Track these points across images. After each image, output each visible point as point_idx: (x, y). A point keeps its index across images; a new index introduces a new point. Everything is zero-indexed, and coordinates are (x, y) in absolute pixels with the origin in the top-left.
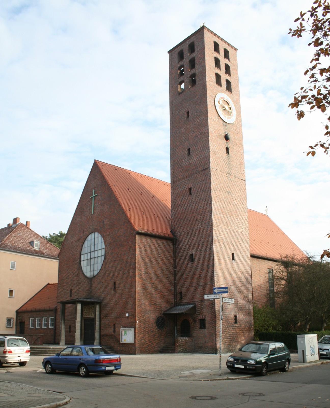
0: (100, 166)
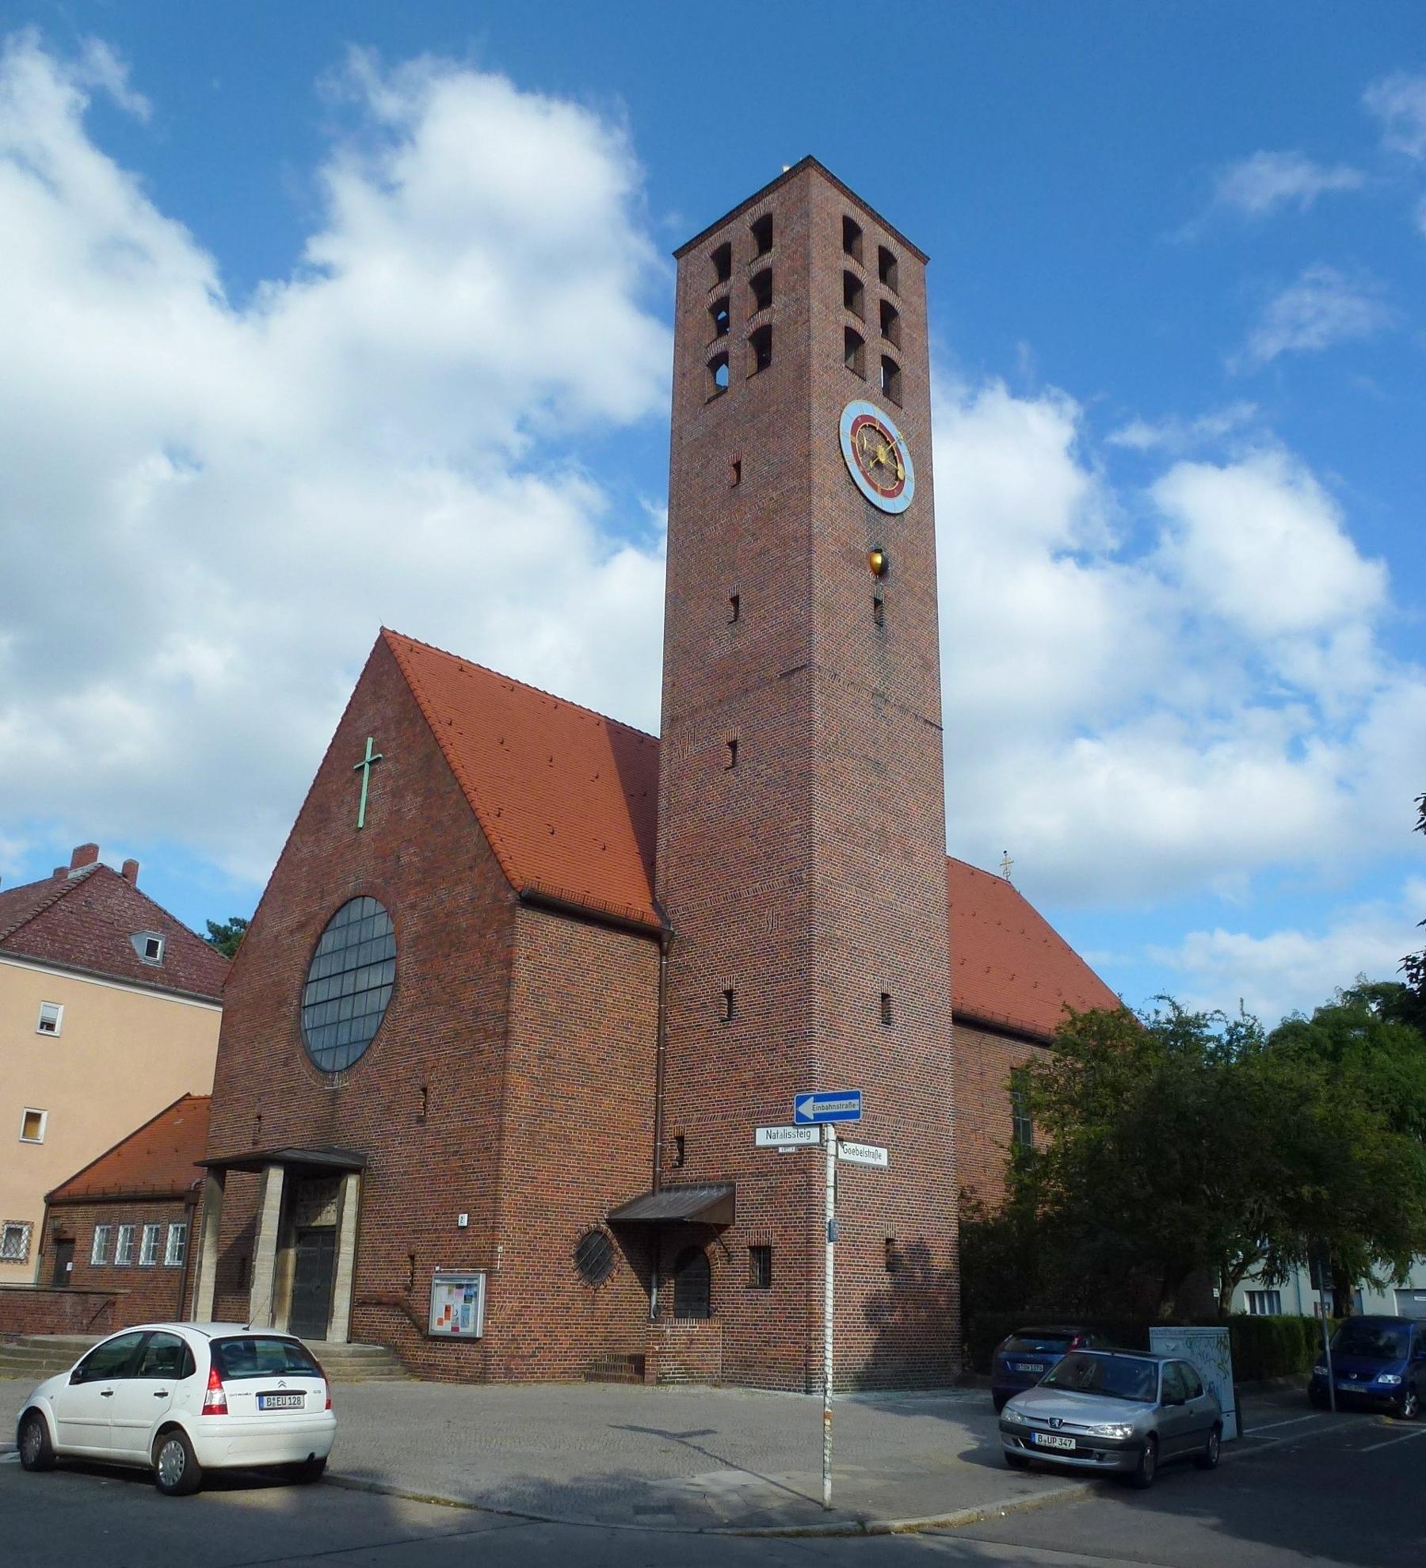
0: (401, 652)
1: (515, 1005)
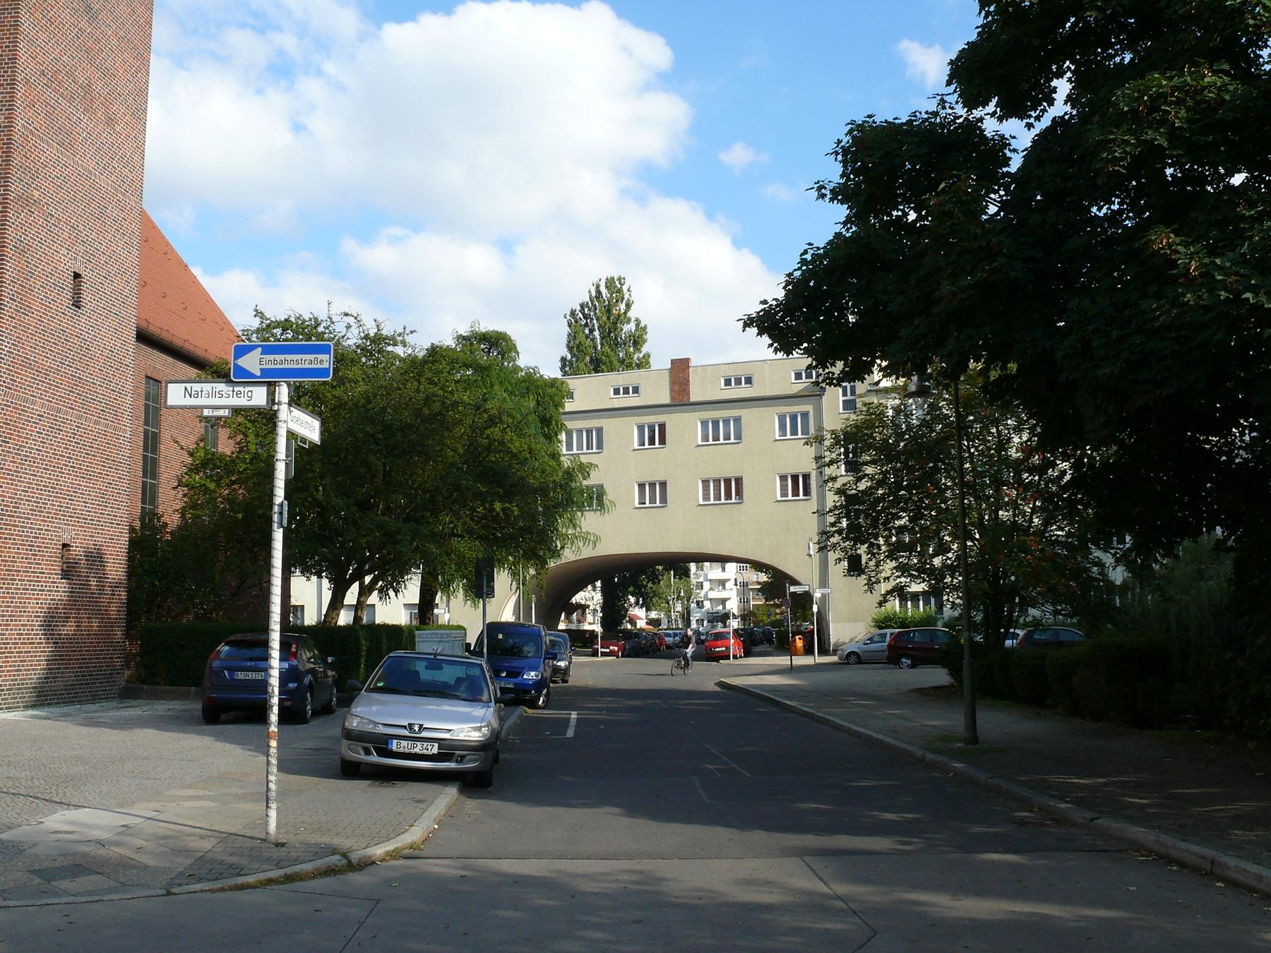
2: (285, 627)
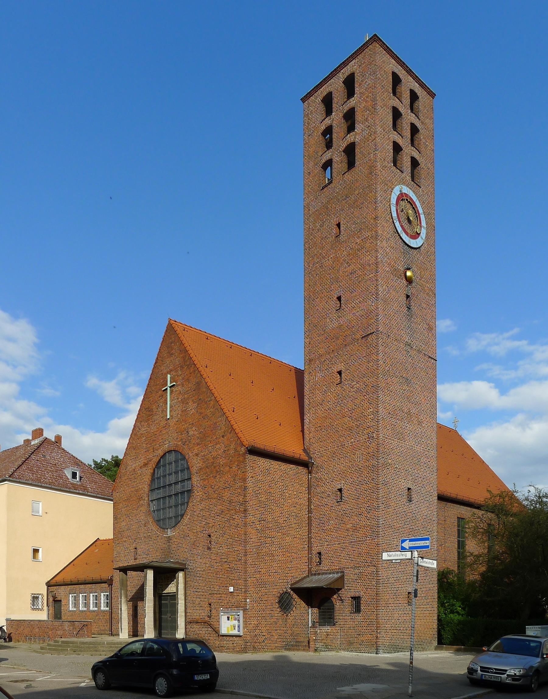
0: (179, 331)
1: (248, 499)
2: (141, 656)
